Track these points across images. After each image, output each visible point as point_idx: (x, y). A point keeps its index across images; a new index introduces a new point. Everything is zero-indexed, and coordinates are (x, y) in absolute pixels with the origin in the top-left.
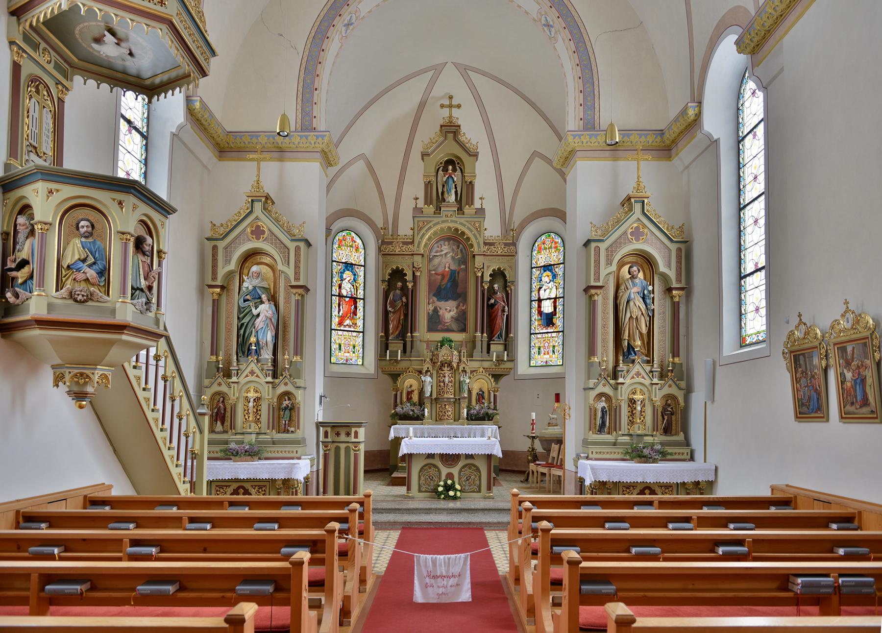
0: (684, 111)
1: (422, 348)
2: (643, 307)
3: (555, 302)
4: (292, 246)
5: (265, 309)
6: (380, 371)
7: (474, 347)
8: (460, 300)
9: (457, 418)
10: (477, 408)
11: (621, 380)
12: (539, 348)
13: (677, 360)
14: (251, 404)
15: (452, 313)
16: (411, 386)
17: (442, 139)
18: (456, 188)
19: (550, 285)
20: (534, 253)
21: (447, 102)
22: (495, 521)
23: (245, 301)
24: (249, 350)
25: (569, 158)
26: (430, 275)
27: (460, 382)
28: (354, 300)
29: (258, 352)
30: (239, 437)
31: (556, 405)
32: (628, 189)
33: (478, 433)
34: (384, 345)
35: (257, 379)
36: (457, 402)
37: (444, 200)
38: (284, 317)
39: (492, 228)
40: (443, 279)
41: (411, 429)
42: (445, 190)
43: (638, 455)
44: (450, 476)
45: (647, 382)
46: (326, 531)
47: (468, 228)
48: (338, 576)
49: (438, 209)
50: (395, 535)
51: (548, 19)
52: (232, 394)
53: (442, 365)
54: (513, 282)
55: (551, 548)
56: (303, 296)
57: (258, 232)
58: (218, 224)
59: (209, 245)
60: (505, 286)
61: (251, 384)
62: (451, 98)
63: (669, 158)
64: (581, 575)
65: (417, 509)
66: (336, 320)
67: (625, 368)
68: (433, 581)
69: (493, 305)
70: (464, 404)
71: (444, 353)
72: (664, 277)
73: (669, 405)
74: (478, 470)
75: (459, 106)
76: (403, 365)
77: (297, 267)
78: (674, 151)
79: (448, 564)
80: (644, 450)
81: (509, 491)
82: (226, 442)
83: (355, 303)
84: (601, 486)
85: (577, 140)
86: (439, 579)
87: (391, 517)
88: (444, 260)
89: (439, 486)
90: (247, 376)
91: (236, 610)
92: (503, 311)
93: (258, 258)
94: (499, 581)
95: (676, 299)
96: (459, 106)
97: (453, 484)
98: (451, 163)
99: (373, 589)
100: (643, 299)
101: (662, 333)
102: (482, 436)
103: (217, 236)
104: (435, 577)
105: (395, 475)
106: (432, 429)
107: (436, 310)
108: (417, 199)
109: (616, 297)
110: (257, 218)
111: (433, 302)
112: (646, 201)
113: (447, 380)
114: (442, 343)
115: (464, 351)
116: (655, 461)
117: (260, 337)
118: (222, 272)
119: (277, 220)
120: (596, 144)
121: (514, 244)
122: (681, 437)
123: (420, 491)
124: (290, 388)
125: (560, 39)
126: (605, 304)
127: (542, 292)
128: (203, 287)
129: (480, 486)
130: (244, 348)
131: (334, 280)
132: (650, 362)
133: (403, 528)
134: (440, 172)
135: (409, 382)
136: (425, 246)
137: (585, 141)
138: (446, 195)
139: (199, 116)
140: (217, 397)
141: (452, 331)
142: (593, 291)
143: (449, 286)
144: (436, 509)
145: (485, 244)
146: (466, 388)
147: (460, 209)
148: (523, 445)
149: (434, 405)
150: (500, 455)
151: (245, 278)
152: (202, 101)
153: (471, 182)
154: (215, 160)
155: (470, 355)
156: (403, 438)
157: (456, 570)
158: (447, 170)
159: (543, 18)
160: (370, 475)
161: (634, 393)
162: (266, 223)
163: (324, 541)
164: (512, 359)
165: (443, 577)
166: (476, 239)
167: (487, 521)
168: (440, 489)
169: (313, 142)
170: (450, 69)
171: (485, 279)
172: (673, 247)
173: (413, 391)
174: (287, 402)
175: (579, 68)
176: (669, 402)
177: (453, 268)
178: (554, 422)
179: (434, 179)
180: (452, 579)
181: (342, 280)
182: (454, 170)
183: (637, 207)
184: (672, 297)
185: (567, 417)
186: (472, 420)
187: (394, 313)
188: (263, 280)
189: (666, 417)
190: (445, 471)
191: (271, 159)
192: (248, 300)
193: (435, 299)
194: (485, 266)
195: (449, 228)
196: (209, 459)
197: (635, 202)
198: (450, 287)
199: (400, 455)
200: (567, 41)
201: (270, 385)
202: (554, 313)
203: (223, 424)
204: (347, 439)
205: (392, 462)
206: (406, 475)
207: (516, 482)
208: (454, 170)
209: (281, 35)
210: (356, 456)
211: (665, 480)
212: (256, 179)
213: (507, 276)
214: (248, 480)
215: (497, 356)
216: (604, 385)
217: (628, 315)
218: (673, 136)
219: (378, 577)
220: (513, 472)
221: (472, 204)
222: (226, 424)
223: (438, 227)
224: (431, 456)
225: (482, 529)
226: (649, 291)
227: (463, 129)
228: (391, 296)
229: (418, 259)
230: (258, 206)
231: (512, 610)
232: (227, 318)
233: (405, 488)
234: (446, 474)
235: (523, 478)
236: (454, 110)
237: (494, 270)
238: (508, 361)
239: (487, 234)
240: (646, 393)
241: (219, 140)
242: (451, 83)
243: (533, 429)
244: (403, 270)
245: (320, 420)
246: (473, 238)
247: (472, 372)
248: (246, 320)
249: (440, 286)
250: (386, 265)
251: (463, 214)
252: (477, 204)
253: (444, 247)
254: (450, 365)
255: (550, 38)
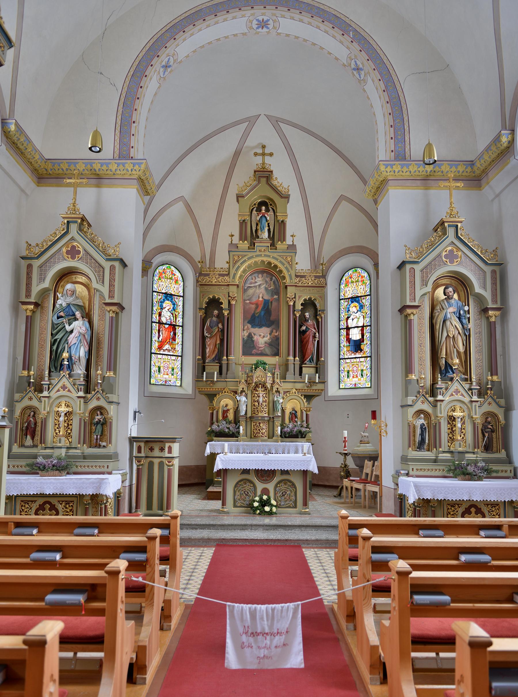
0: (497, 139)
2: (459, 326)
3: (362, 330)
4: (107, 265)
5: (79, 326)
6: (197, 391)
7: (287, 370)
8: (273, 327)
9: (271, 436)
10: (290, 426)
11: (440, 397)
12: (348, 372)
13: (495, 378)
14: (62, 419)
15: (266, 339)
16: (227, 406)
17: (255, 183)
18: (269, 226)
19: (357, 315)
21: (260, 151)
22: (313, 538)
23: (58, 318)
24: (61, 365)
25: (380, 189)
26: (245, 304)
27: (274, 402)
28: (173, 327)
29: (70, 367)
30: (48, 451)
31: (373, 422)
32: (441, 213)
33: (292, 449)
34: (201, 368)
35: (68, 394)
36: (271, 420)
37: (258, 237)
38: (98, 334)
40: (257, 307)
41: (226, 444)
42: (259, 228)
43: (461, 472)
44: (265, 491)
45: (467, 399)
46: (107, 572)
47: (281, 262)
48: (125, 627)
49: (252, 245)
50: (209, 553)
51: (358, 63)
52: (43, 409)
53: (257, 386)
54: (323, 311)
55: (411, 597)
56: (117, 313)
57: (73, 252)
58: (33, 244)
59: (24, 264)
60: (316, 315)
61: (62, 401)
62: (264, 147)
63: (479, 187)
64: (491, 663)
65: (232, 525)
66: (155, 345)
67: (443, 386)
68: (251, 639)
69: (304, 332)
70: (278, 422)
71: (258, 375)
72: (479, 298)
73: (489, 423)
74: (294, 485)
75: (271, 155)
76: (219, 386)
77: (111, 285)
78: (483, 181)
79: (272, 617)
80: (469, 467)
81: (325, 510)
82: (35, 457)
83: (174, 330)
84: (425, 506)
85: (389, 169)
86: (260, 637)
87: (205, 534)
89: (254, 501)
90: (58, 391)
91: (35, 632)
92: (314, 337)
93: (74, 278)
94: (326, 614)
95: (493, 319)
96: (271, 155)
97: (269, 499)
98: (264, 204)
99: (179, 624)
100: (459, 318)
101: (479, 352)
102: (296, 452)
103: (32, 255)
104: (254, 634)
106: (247, 445)
107: (250, 336)
108: (232, 236)
109: (432, 317)
110: (72, 239)
111: (248, 329)
112: (459, 225)
113: (261, 400)
114: (257, 366)
116: (480, 479)
117: (73, 353)
118: (36, 289)
119: (93, 241)
120: (408, 173)
121: (324, 276)
122: (503, 454)
123: (235, 506)
124: (102, 403)
125: (370, 81)
126: (420, 324)
127: (350, 321)
128: (17, 304)
129: (295, 502)
130: (56, 364)
131: (154, 309)
132: (468, 380)
133: (218, 545)
134: (254, 212)
135: (225, 402)
136: (241, 277)
137: (397, 170)
138: (259, 232)
139: (15, 138)
140: (28, 412)
142: (409, 311)
143: (263, 313)
144: (252, 525)
145: (297, 276)
146: (280, 407)
147: (273, 245)
148: (336, 462)
149: (249, 423)
150: (316, 471)
151: (59, 295)
152: (17, 124)
153: (282, 221)
154: (33, 185)
155: (283, 377)
156: (218, 454)
157: (284, 625)
158: (261, 210)
159: (353, 63)
161: (454, 411)
162: (81, 244)
163: (104, 585)
164: (323, 382)
165: (264, 634)
166: (288, 271)
167: (305, 538)
168: (256, 504)
169: (130, 169)
170: (263, 122)
171: (297, 308)
172: (488, 270)
173: (228, 410)
174: (99, 417)
175: (389, 105)
176: (489, 419)
177: (267, 297)
178: (366, 439)
179: (248, 218)
180: (277, 638)
181: (162, 309)
182: (267, 210)
183: (451, 232)
184: (488, 318)
185: (383, 434)
186: (286, 437)
188: (77, 298)
189: (487, 435)
190: (260, 486)
191: (87, 185)
192: (62, 317)
193: (249, 326)
194: (297, 297)
195: (263, 262)
196: (10, 473)
197: (449, 226)
199: (215, 470)
200: (377, 81)
201: (82, 400)
202: (362, 340)
203: (33, 438)
205: (208, 477)
206: (221, 490)
207: (329, 496)
208: (267, 210)
209: (101, 73)
210: (169, 471)
211: (492, 498)
212: (72, 202)
214: (54, 496)
215: (309, 379)
216: (423, 402)
217: (445, 334)
218: (485, 165)
219: (187, 606)
221: (284, 240)
222: (36, 438)
223: (253, 261)
224: (246, 471)
225: (299, 547)
226: (465, 311)
227: (275, 174)
228: (208, 323)
229: (233, 289)
230: (74, 228)
231: (346, 658)
232: (41, 334)
234: (260, 489)
235: (336, 493)
236: (266, 157)
237: (305, 300)
238: (319, 382)
239: (298, 267)
240: (466, 410)
241: (36, 165)
242: (263, 134)
243: (345, 447)
244: (219, 299)
245: (134, 434)
246: (285, 271)
248: (59, 336)
250: (203, 294)
251: (276, 249)
252: (289, 241)
253: (257, 279)
254: (264, 386)
255: (359, 81)
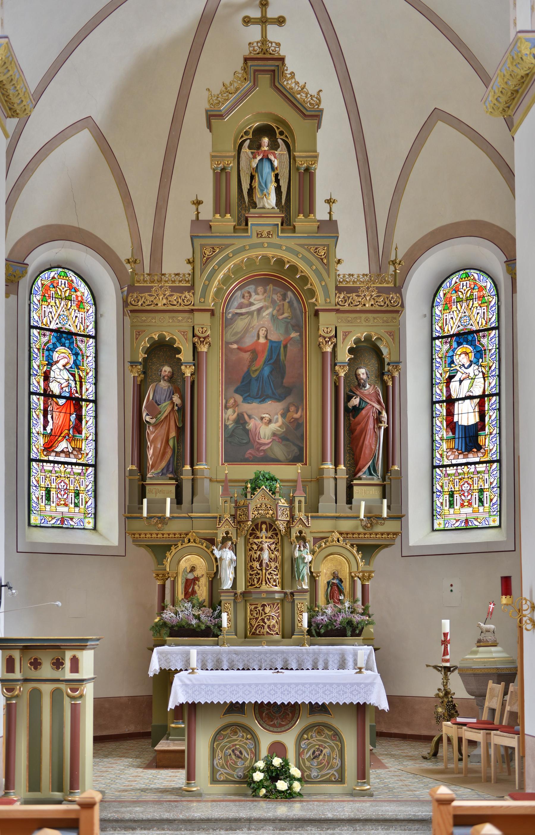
1: (213, 495)
3: (481, 405)
6: (129, 539)
7: (320, 491)
8: (289, 399)
9: (288, 633)
10: (329, 611)
15: (274, 426)
17: (247, 85)
18: (277, 181)
19: (470, 371)
20: (437, 311)
27: (293, 560)
28: (75, 403)
31: (504, 600)
33: (333, 661)
39: (352, 259)
40: (253, 359)
41: (194, 651)
42: (256, 184)
44: (278, 749)
47: (304, 258)
49: (243, 223)
53: (257, 527)
66: (39, 442)
69: (356, 410)
70: (302, 603)
71: (257, 504)
75: (281, 21)
83: (78, 409)
88: (255, 322)
89: (254, 770)
92: (378, 420)
96: (281, 21)
97: (285, 765)
98: (268, 132)
105: (163, 745)
106: (237, 653)
107: (241, 421)
108: (198, 203)
113: (266, 556)
114: (256, 484)
115: (300, 498)
123: (214, 780)
127: (454, 385)
129: (342, 770)
131: (35, 365)
134: (245, 150)
138: (258, 195)
141: (275, 461)
144: (249, 821)
146: (305, 571)
147: (287, 223)
148: (426, 685)
149: (241, 606)
150: (384, 705)
153: (307, 170)
155: (313, 508)
156: (176, 671)
158: (259, 146)
160: (111, 746)
164: (399, 516)
166: (321, 279)
173: (197, 579)
177: (273, 337)
178: (489, 637)
179: (232, 165)
181: (50, 364)
182: (274, 146)
186: (319, 635)
187: (156, 425)
190: (266, 739)
193: (239, 398)
195: (266, 259)
198: (269, 376)
199: (171, 705)
202: (481, 425)
204: (56, 675)
205: (156, 721)
206: (184, 747)
207: (412, 758)
208: (274, 146)
210: (76, 711)
213: (385, 351)
215: (368, 510)
220: (404, 737)
221: (312, 210)
224: (236, 708)
227: (291, 65)
228: (150, 394)
233: (182, 774)
235: (426, 749)
237: (357, 341)
238: (390, 518)
239: (342, 270)
243: (445, 653)
244: (173, 341)
246: (313, 278)
247: (316, 540)
249: (248, 374)
250: (137, 334)
251: (294, 230)
252: (321, 212)
253: (254, 297)
254: (272, 527)
